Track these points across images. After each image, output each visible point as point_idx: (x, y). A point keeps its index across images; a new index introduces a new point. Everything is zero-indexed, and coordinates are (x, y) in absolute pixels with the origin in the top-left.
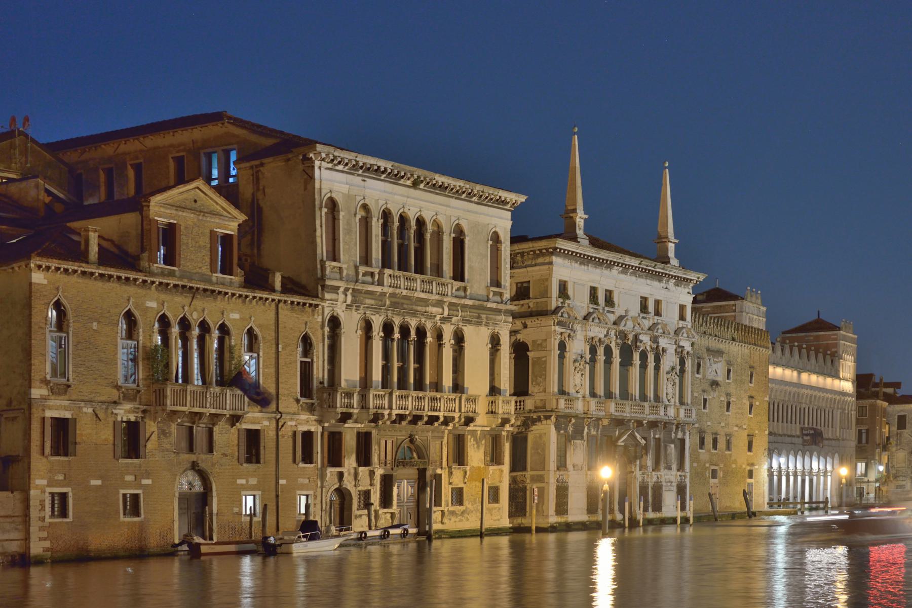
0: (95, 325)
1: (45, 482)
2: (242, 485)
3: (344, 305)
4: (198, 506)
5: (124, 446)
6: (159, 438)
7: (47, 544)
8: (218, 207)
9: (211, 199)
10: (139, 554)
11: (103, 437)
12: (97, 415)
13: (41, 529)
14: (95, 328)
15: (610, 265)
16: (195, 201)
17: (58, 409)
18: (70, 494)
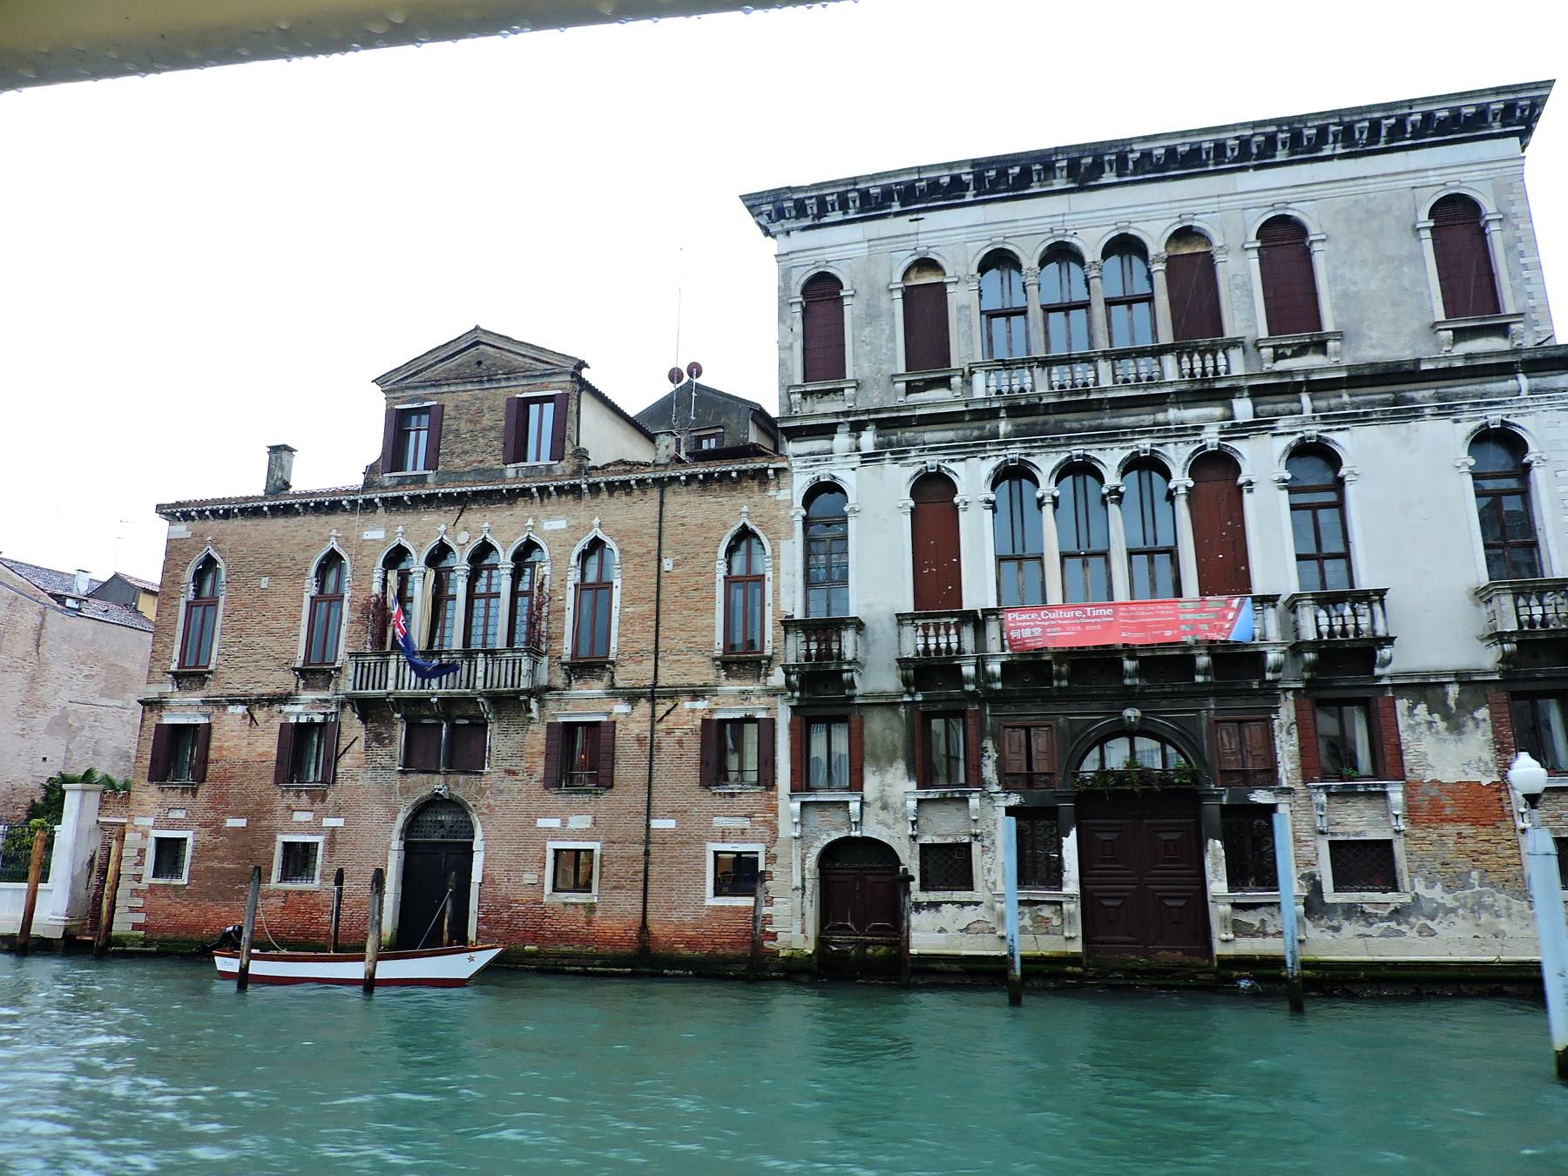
6: (368, 747)
14: (264, 586)
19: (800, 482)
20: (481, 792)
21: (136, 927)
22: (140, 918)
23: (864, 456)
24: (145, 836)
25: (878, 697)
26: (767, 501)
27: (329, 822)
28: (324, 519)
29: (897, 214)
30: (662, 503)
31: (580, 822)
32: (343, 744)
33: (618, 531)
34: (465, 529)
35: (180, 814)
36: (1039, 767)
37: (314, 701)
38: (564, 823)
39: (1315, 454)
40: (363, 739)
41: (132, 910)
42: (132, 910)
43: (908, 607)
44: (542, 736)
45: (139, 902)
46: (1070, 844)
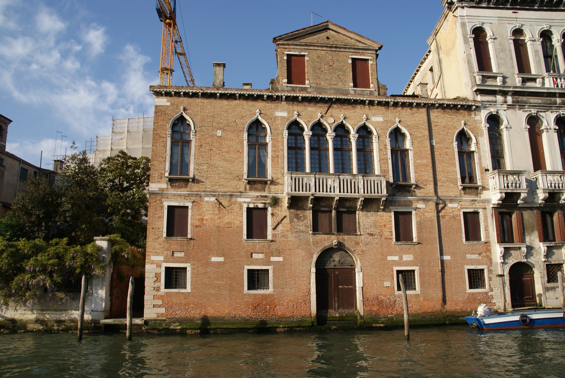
0: (219, 133)
1: (161, 258)
2: (394, 261)
3: (505, 106)
4: (332, 279)
5: (451, 312)
6: (291, 221)
7: (162, 310)
8: (353, 41)
9: (344, 35)
10: (262, 329)
11: (227, 221)
12: (220, 203)
13: (155, 297)
14: (220, 135)
15: (359, 222)
16: (328, 38)
17: (176, 198)
18: (189, 269)
20: (357, 243)
23: (508, 105)
26: (471, 120)
27: (273, 259)
31: (407, 258)
33: (408, 125)
34: (332, 116)
37: (257, 197)
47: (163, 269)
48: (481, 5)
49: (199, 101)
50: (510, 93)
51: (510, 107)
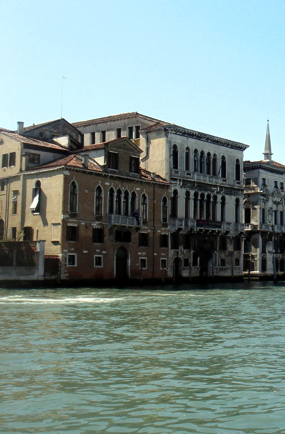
6: (109, 235)
14: (86, 192)
19: (173, 189)
21: (67, 277)
22: (67, 275)
24: (66, 254)
25: (173, 387)
27: (104, 252)
28: (97, 177)
29: (186, 136)
30: (154, 189)
32: (105, 234)
35: (73, 249)
36: (196, 246)
38: (142, 253)
39: (223, 199)
40: (108, 233)
41: (65, 273)
42: (65, 273)
43: (35, 125)
44: (138, 235)
45: (66, 271)
46: (199, 258)
47: (68, 256)
48: (177, 133)
49: (80, 174)
50: (178, 180)
51: (181, 187)
